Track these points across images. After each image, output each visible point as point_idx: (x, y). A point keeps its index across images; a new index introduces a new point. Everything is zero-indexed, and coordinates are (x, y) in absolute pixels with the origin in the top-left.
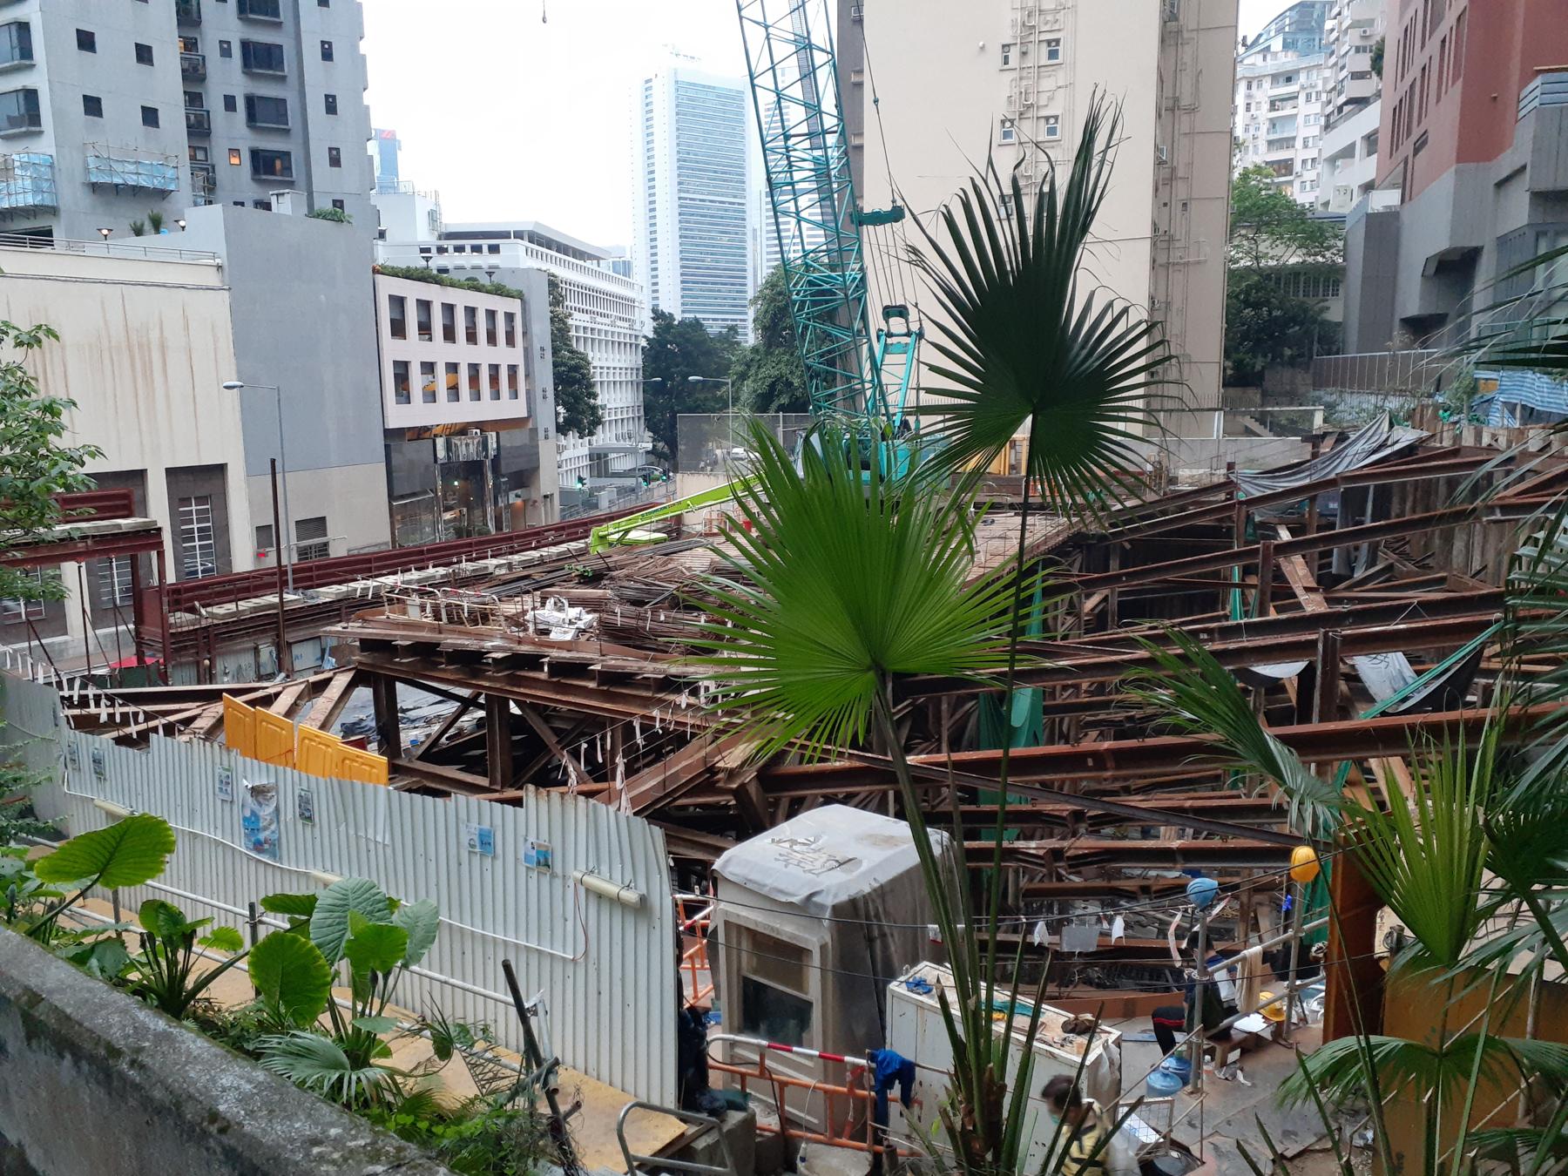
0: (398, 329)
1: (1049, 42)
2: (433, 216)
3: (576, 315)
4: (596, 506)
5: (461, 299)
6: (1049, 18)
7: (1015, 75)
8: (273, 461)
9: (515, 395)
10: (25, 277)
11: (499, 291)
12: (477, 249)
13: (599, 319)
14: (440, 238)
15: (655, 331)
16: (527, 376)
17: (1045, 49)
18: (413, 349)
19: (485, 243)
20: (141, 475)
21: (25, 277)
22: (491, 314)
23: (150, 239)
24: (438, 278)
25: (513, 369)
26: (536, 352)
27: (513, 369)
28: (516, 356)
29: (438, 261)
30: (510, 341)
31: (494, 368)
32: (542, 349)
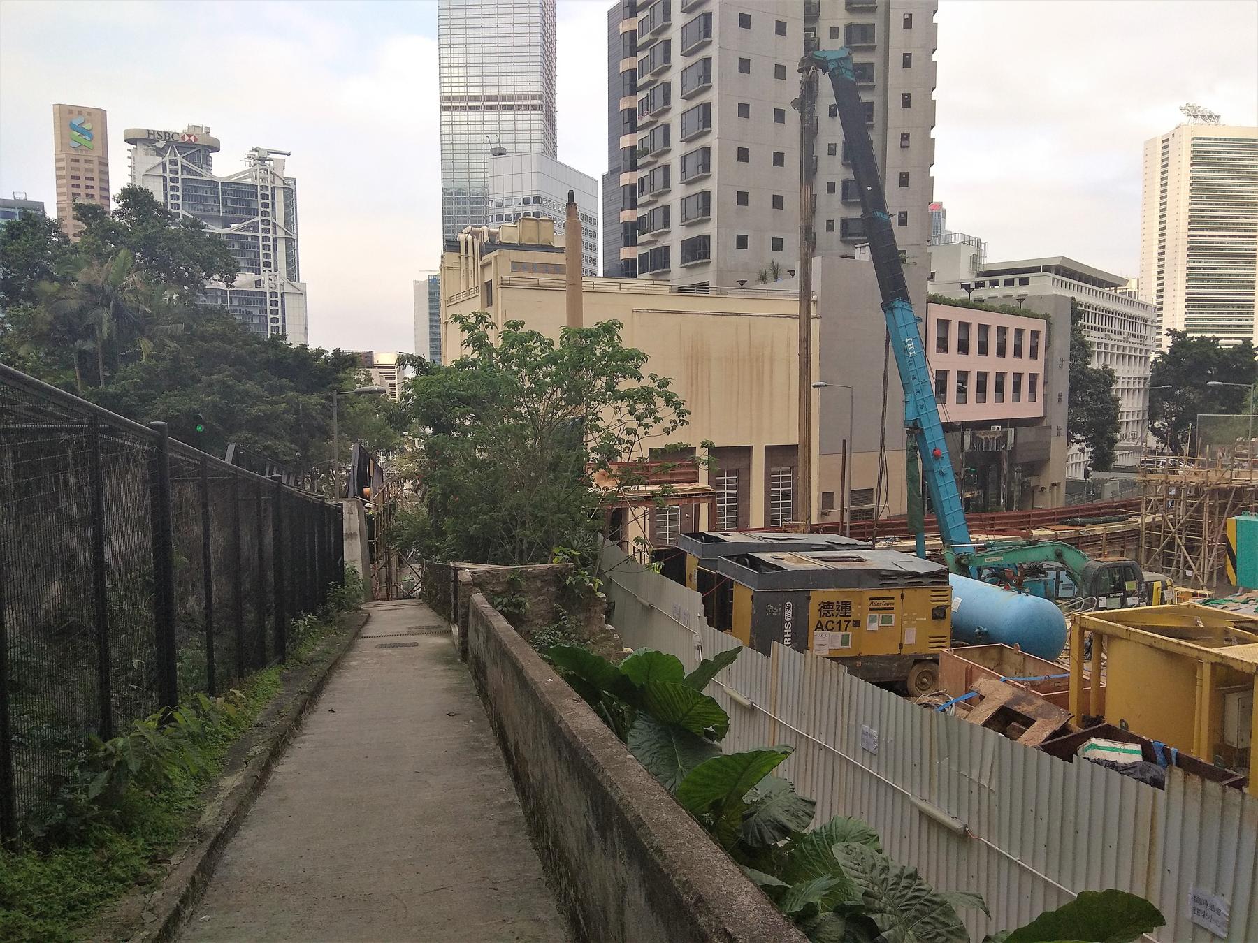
0: (943, 346)
2: (974, 259)
3: (1093, 333)
4: (1099, 496)
5: (995, 321)
8: (845, 442)
9: (1033, 398)
10: (692, 313)
11: (1027, 314)
12: (1009, 283)
13: (1113, 336)
15: (1171, 349)
16: (1045, 383)
18: (952, 362)
19: (1017, 277)
20: (748, 450)
21: (692, 313)
23: (772, 285)
26: (1056, 363)
27: (1033, 377)
28: (1037, 366)
29: (977, 294)
30: (1034, 354)
31: (1018, 377)
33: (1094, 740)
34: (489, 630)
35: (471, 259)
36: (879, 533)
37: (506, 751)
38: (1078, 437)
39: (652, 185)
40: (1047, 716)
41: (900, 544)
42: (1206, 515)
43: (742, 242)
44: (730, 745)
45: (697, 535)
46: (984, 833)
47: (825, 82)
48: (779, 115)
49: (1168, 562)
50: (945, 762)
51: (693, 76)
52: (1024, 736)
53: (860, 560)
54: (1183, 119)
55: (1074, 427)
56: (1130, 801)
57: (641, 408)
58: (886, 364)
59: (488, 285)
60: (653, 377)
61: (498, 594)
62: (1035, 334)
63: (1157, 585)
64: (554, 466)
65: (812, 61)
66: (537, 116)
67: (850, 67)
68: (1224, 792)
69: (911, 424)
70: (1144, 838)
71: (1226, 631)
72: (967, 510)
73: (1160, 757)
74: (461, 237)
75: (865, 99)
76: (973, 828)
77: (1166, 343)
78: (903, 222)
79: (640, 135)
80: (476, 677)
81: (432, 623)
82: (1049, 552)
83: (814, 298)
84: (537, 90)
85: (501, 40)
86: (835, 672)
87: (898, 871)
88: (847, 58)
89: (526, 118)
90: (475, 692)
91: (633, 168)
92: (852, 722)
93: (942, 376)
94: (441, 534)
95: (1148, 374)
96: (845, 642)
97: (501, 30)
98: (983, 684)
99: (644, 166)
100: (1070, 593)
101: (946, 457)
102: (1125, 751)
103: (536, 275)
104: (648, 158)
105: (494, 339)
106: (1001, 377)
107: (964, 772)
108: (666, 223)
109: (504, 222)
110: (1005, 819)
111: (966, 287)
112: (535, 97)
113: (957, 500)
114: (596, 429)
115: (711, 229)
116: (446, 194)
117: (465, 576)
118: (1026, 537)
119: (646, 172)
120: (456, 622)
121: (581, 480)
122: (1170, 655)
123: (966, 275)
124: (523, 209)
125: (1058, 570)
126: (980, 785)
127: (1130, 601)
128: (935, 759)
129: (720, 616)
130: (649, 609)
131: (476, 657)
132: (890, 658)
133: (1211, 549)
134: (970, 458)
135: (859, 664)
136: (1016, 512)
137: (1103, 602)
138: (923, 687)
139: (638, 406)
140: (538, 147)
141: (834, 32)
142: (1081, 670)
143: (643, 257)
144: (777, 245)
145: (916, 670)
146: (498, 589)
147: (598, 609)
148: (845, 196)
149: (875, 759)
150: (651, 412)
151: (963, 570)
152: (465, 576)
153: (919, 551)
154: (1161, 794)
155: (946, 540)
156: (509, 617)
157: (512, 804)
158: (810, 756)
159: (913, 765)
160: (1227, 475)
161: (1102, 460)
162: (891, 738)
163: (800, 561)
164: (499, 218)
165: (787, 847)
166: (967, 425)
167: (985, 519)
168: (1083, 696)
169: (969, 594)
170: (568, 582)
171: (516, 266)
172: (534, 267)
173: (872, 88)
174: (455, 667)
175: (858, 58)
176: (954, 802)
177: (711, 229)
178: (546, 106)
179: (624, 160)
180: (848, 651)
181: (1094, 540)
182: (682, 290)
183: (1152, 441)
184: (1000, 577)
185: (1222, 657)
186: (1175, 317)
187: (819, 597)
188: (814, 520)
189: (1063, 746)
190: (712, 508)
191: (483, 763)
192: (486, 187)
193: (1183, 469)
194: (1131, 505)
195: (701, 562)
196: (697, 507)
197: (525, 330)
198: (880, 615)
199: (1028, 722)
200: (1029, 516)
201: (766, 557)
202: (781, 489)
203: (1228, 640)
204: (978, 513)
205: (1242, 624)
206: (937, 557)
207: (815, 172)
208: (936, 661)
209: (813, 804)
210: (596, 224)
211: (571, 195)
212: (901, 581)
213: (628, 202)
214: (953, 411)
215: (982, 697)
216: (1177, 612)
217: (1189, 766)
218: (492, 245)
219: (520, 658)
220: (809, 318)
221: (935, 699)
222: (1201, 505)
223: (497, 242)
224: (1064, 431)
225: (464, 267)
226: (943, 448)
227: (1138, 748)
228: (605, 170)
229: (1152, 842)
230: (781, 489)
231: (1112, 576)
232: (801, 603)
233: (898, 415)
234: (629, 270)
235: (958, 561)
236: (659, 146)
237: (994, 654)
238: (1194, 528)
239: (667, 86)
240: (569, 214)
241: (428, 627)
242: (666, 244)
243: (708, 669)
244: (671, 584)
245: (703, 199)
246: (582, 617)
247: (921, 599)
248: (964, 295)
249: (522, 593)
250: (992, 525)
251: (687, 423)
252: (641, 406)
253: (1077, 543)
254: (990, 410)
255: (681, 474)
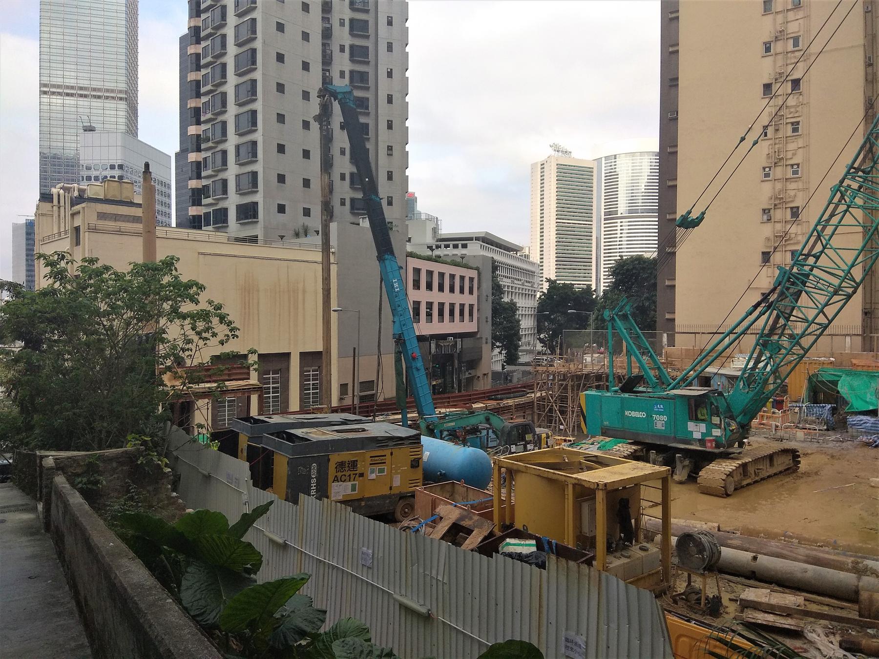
0: (417, 286)
1: (792, 124)
3: (505, 279)
4: (511, 381)
5: (448, 270)
6: (792, 110)
7: (769, 142)
10: (245, 257)
12: (456, 246)
14: (437, 241)
17: (790, 127)
18: (422, 296)
19: (460, 243)
20: (288, 355)
21: (245, 257)
22: (462, 278)
23: (302, 240)
24: (437, 259)
25: (471, 306)
26: (484, 298)
27: (471, 306)
29: (437, 252)
30: (471, 292)
32: (487, 296)
33: (508, 540)
34: (66, 506)
35: (62, 209)
36: (378, 411)
37: (78, 603)
38: (498, 344)
39: (214, 163)
40: (480, 527)
41: (391, 417)
42: (570, 391)
43: (281, 209)
44: (264, 576)
45: (248, 419)
46: (440, 612)
47: (336, 107)
48: (306, 125)
49: (550, 421)
50: (415, 567)
51: (243, 90)
52: (467, 542)
53: (364, 430)
54: (551, 152)
55: (495, 338)
56: (527, 579)
57: (201, 325)
58: (381, 296)
59: (77, 229)
60: (210, 302)
61: (78, 475)
62: (471, 280)
63: (544, 436)
64: (131, 369)
65: (327, 91)
66: (123, 105)
67: (352, 98)
68: (579, 567)
69: (397, 336)
70: (536, 604)
71: (580, 463)
72: (434, 393)
73: (546, 547)
74: (54, 191)
75: (358, 115)
76: (434, 611)
77: (546, 286)
78: (390, 203)
79: (203, 127)
80: (56, 544)
81: (20, 502)
82: (482, 418)
83: (332, 250)
84: (122, 86)
85: (93, 47)
86: (343, 512)
87: (378, 653)
88: (350, 92)
89: (113, 106)
90: (55, 556)
91: (199, 150)
92: (355, 547)
93: (417, 304)
94: (29, 428)
95: (536, 305)
96: (353, 489)
97: (93, 40)
98: (441, 510)
99: (207, 150)
100: (494, 444)
101: (420, 359)
102: (526, 545)
103: (119, 224)
104: (210, 144)
105: (73, 270)
106: (452, 306)
107: (427, 572)
108: (225, 191)
109: (93, 182)
110: (454, 601)
111: (430, 248)
112: (121, 92)
113: (427, 386)
114: (163, 340)
115: (258, 198)
116: (43, 157)
117: (49, 462)
118: (468, 408)
119: (209, 154)
120: (40, 500)
121: (153, 379)
122: (551, 481)
123: (430, 240)
124: (109, 173)
125: (488, 429)
126: (437, 580)
127: (529, 447)
128: (409, 565)
129: (262, 477)
130: (208, 478)
131: (57, 528)
132: (383, 497)
133: (573, 412)
134: (435, 358)
135: (363, 504)
136: (463, 392)
137: (514, 448)
138: (405, 515)
139: (198, 324)
140: (123, 128)
141: (342, 74)
142: (500, 493)
143: (207, 215)
144: (307, 212)
145: (401, 503)
146: (79, 471)
147: (165, 481)
148: (352, 183)
149: (370, 571)
150: (207, 330)
151: (431, 433)
152: (49, 462)
153: (404, 422)
154: (544, 572)
155: (421, 413)
156: (87, 494)
157: (82, 646)
158: (326, 575)
159: (395, 572)
160: (580, 367)
161: (511, 359)
162: (381, 555)
163: (324, 434)
164: (89, 178)
165: (308, 645)
166: (433, 337)
167: (446, 398)
168: (502, 511)
169: (437, 450)
170: (139, 462)
171: (102, 216)
172: (116, 217)
173: (368, 114)
174: (38, 537)
175: (358, 93)
176: (421, 595)
177: (258, 198)
178: (129, 99)
179: (191, 144)
180: (356, 495)
181: (508, 408)
182: (238, 240)
183: (539, 347)
184: (454, 436)
185: (579, 480)
186: (550, 271)
187: (335, 458)
188: (335, 403)
189: (489, 547)
190: (260, 398)
191: (58, 615)
192: (78, 154)
193: (557, 363)
194: (529, 386)
195: (250, 439)
196: (249, 398)
197: (99, 265)
198: (377, 468)
199: (469, 532)
200: (470, 395)
201: (298, 432)
202: (311, 382)
203: (582, 470)
204: (441, 394)
205: (589, 458)
206: (415, 426)
207: (331, 165)
208: (413, 496)
209: (325, 612)
210: (169, 187)
211: (147, 165)
212: (391, 443)
213: (195, 173)
214: (424, 328)
215: (441, 518)
216: (555, 453)
217: (562, 552)
218: (81, 198)
219: (88, 527)
220: (329, 264)
221: (413, 522)
222: (567, 385)
223: (86, 196)
224: (490, 340)
225: (56, 214)
226: (417, 353)
227: (534, 542)
228: (178, 149)
229: (540, 606)
230: (311, 382)
231: (518, 431)
232: (323, 465)
233: (389, 331)
234: (196, 223)
235: (428, 427)
236: (218, 137)
237: (448, 488)
238: (563, 399)
239: (224, 95)
240: (145, 179)
241: (14, 506)
242: (225, 206)
243: (247, 521)
244: (227, 458)
245: (253, 176)
246: (150, 488)
247: (404, 454)
248: (429, 253)
249: (101, 473)
250: (449, 402)
251: (237, 337)
252: (201, 324)
253: (498, 411)
254: (447, 327)
255: (237, 374)
